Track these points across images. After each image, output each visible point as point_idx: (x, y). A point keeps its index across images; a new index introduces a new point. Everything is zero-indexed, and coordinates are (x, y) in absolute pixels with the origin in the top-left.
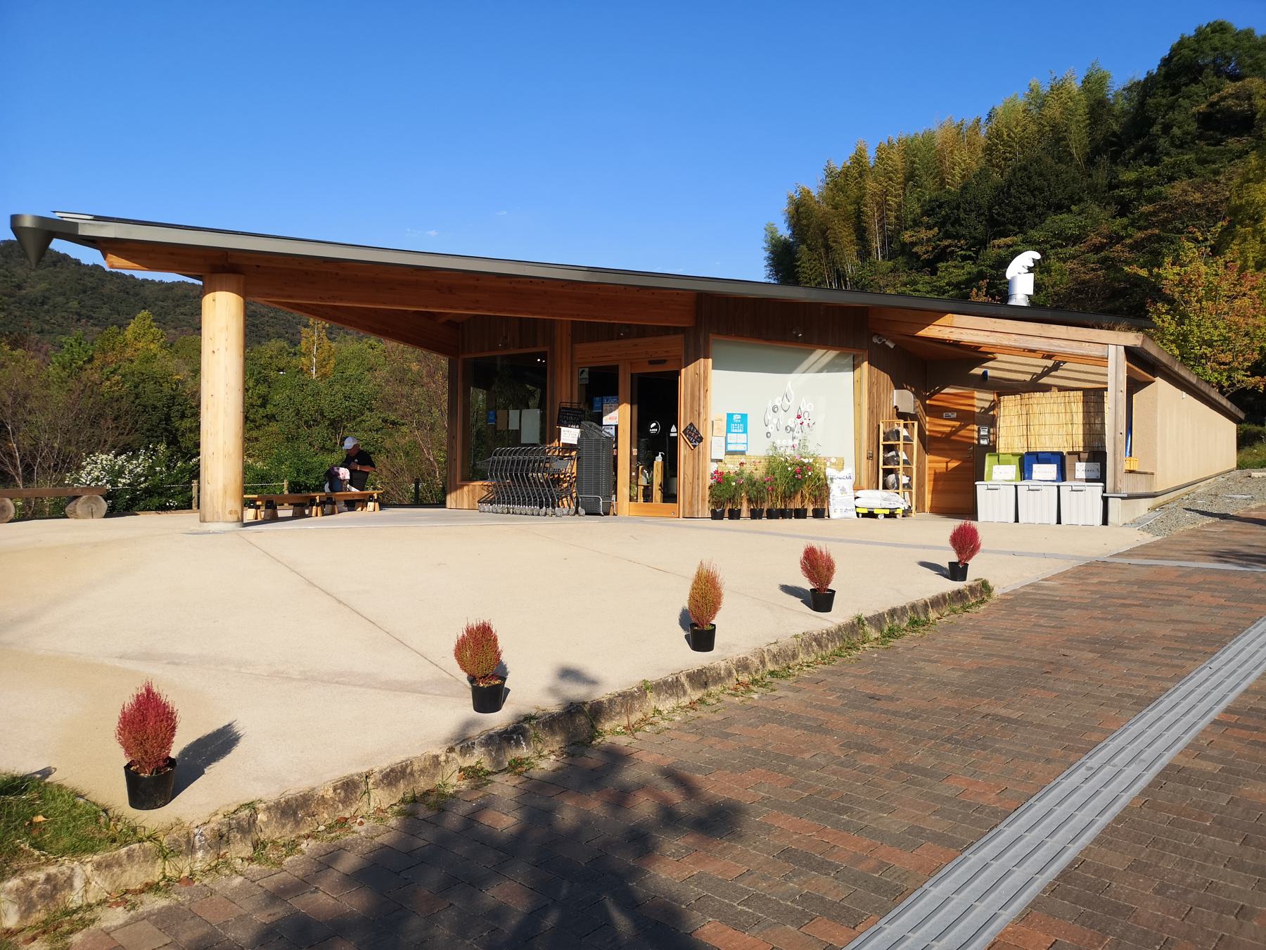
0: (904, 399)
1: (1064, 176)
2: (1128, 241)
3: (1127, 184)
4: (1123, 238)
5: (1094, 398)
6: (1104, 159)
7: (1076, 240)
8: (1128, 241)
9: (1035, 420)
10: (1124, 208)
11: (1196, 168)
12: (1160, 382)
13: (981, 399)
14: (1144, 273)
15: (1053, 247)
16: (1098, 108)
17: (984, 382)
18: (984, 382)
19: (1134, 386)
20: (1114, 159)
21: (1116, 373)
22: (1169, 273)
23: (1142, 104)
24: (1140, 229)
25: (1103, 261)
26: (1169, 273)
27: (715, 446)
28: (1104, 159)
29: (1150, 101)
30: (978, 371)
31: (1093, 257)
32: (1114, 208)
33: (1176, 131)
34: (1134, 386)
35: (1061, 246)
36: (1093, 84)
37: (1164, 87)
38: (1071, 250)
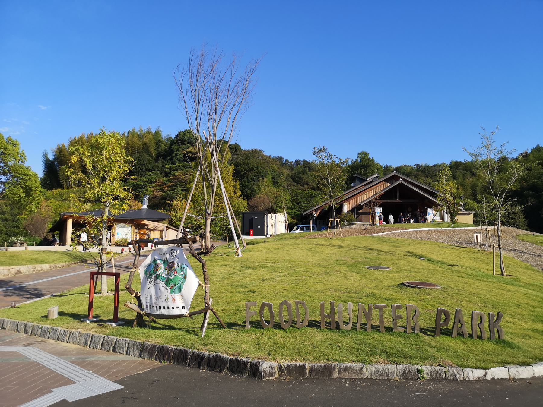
0: (137, 231)
1: (151, 161)
2: (167, 185)
3: (167, 168)
4: (166, 184)
5: (162, 231)
6: (161, 159)
7: (154, 182)
8: (167, 185)
9: (155, 234)
10: (167, 175)
11: (183, 168)
12: (170, 229)
13: (147, 231)
14: (170, 202)
15: (148, 183)
16: (158, 142)
17: (147, 229)
18: (147, 229)
19: (167, 230)
20: (164, 159)
21: (164, 229)
22: (174, 203)
23: (170, 147)
24: (170, 182)
25: (161, 189)
26: (174, 203)
27: (116, 237)
28: (161, 159)
29: (173, 147)
30: (146, 227)
31: (158, 188)
32: (164, 174)
33: (178, 157)
34: (167, 230)
35: (150, 183)
36: (157, 134)
37: (176, 143)
38: (153, 185)
